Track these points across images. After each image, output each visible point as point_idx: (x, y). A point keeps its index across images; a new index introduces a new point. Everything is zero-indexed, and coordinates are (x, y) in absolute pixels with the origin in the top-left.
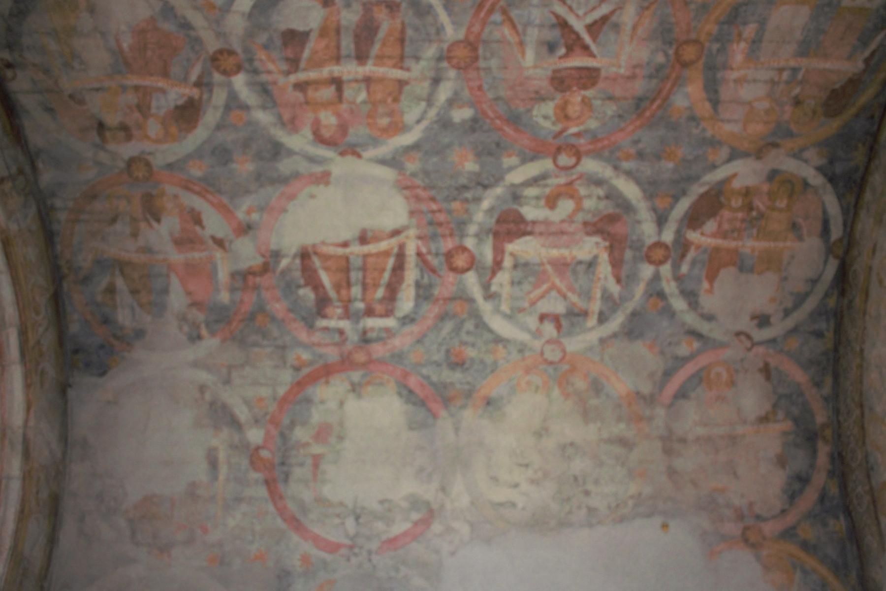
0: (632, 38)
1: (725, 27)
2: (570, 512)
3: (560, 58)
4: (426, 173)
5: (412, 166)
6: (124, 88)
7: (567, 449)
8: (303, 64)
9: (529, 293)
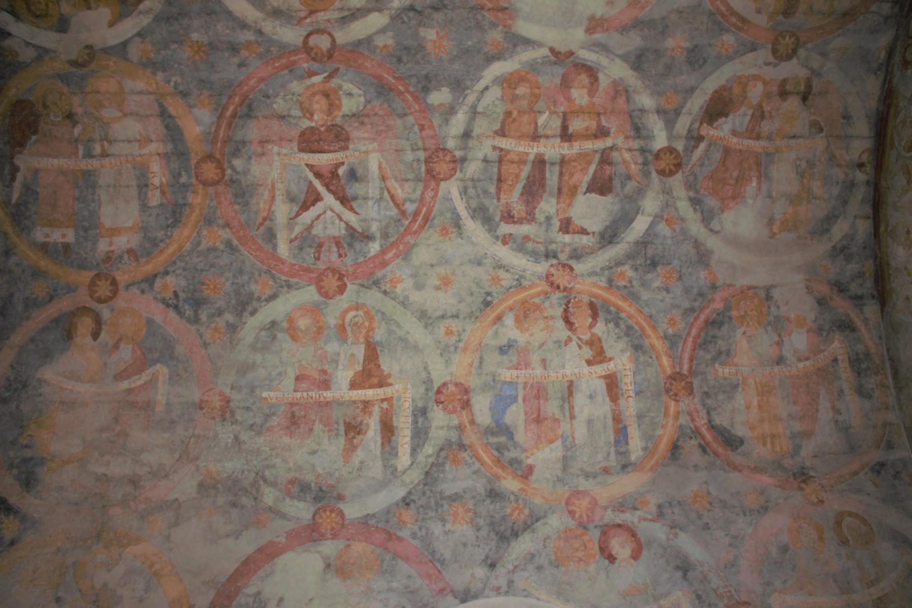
0: (273, 186)
1: (181, 201)
3: (343, 163)
4: (479, 27)
6: (770, 138)
8: (598, 156)
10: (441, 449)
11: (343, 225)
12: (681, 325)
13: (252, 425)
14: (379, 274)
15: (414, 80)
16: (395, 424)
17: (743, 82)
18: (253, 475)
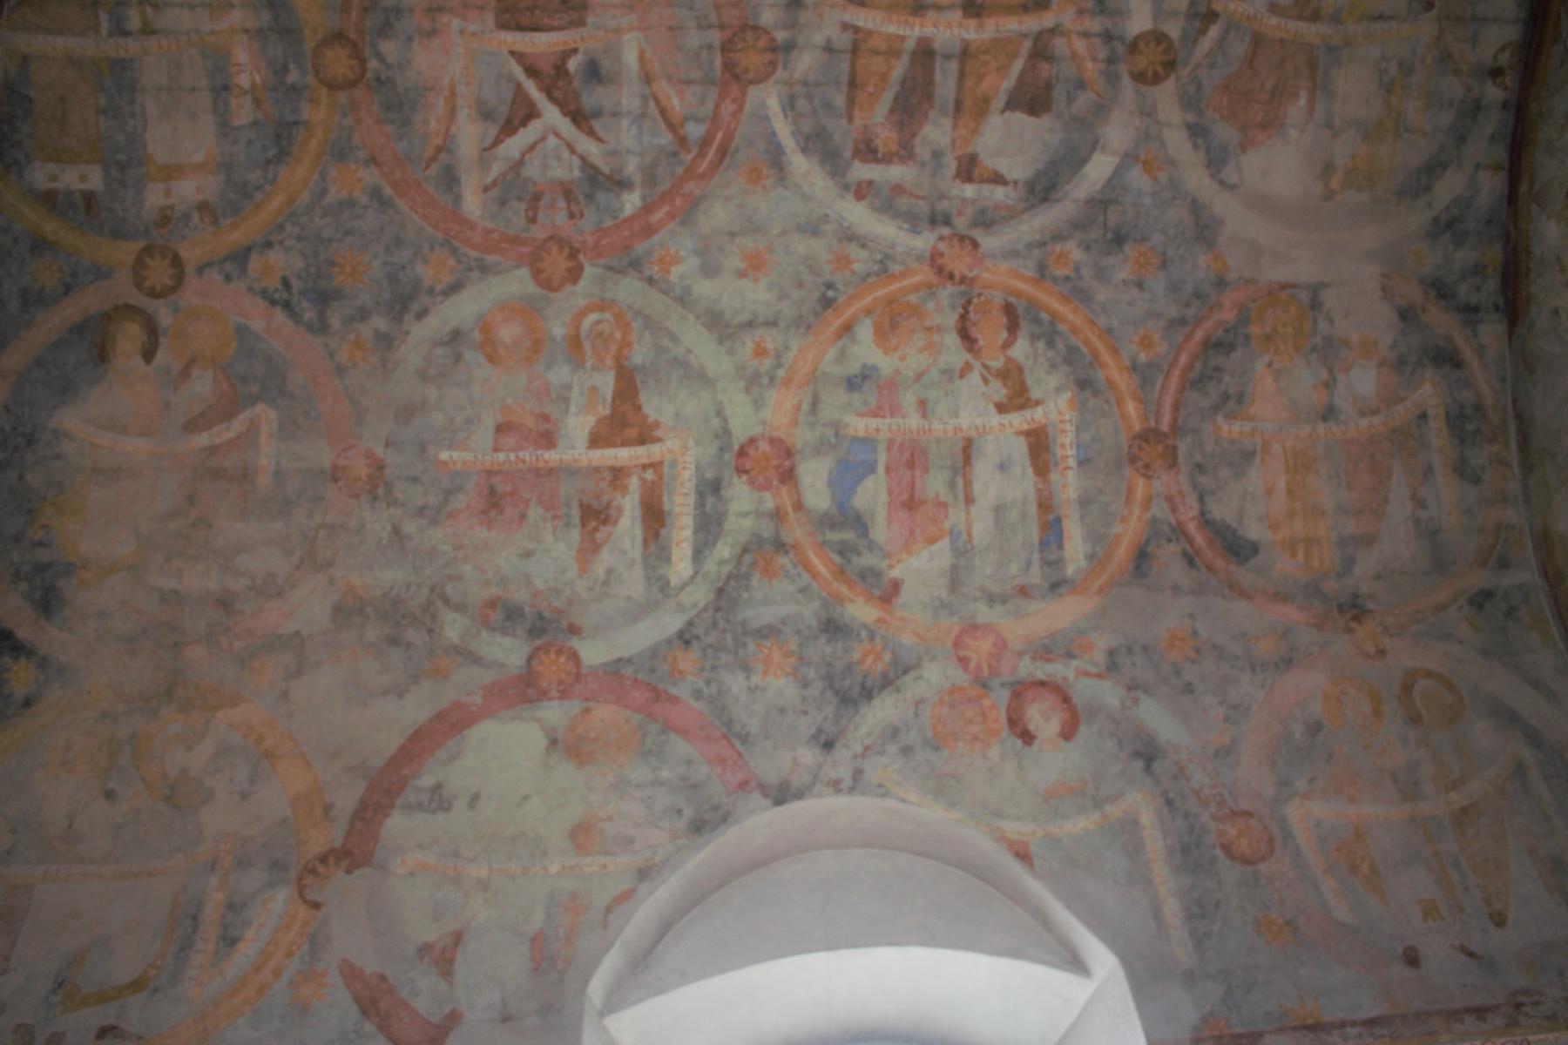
1: (290, 118)
3: (575, 51)
10: (745, 550)
11: (576, 161)
13: (423, 508)
14: (640, 248)
16: (666, 507)
18: (425, 591)
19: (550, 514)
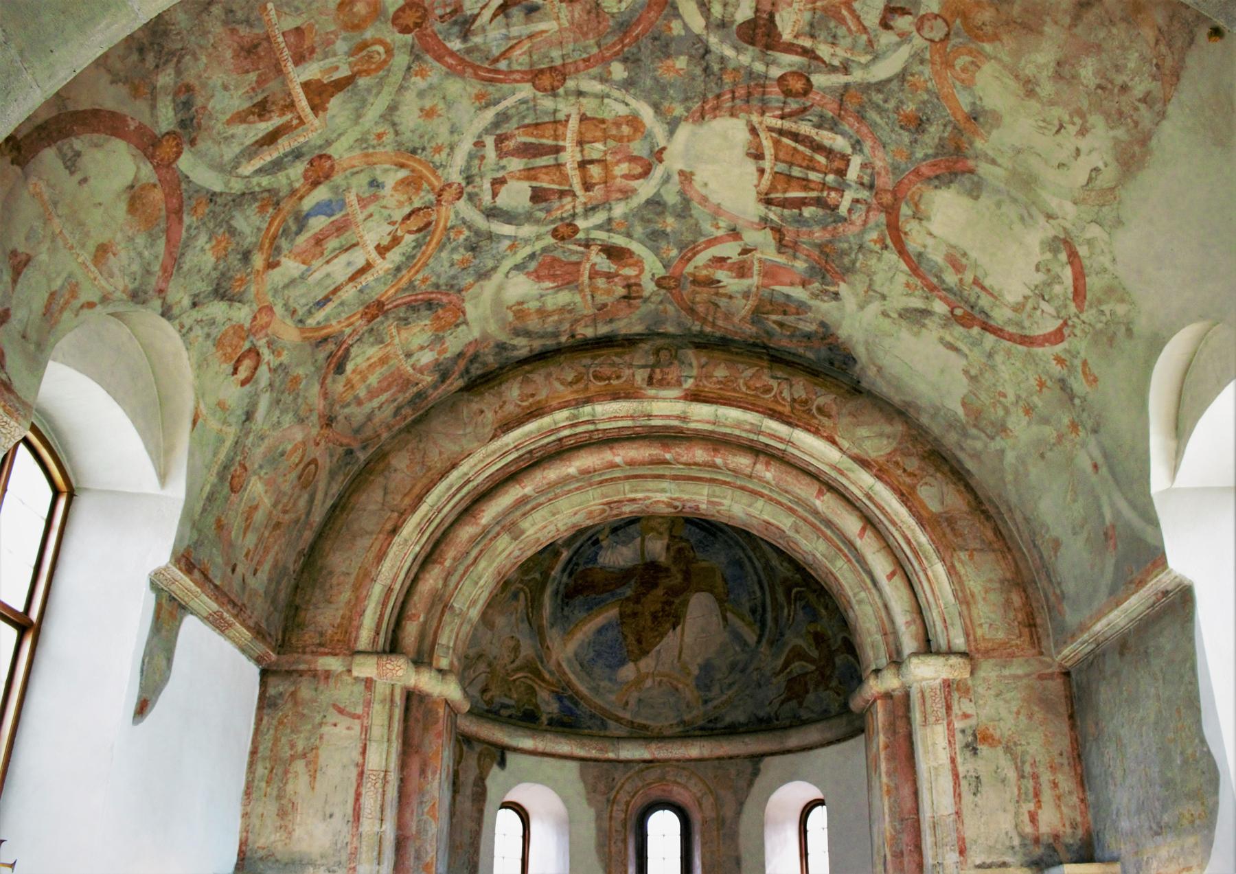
2: (1136, 124)
4: (687, 99)
5: (679, 110)
7: (1063, 71)
9: (849, 29)
10: (269, 191)
11: (476, 11)
12: (423, 287)
13: (231, 11)
14: (428, 57)
15: (635, 50)
16: (280, 141)
17: (639, 263)
18: (180, 46)
19: (254, 85)
